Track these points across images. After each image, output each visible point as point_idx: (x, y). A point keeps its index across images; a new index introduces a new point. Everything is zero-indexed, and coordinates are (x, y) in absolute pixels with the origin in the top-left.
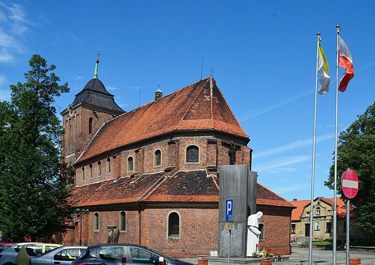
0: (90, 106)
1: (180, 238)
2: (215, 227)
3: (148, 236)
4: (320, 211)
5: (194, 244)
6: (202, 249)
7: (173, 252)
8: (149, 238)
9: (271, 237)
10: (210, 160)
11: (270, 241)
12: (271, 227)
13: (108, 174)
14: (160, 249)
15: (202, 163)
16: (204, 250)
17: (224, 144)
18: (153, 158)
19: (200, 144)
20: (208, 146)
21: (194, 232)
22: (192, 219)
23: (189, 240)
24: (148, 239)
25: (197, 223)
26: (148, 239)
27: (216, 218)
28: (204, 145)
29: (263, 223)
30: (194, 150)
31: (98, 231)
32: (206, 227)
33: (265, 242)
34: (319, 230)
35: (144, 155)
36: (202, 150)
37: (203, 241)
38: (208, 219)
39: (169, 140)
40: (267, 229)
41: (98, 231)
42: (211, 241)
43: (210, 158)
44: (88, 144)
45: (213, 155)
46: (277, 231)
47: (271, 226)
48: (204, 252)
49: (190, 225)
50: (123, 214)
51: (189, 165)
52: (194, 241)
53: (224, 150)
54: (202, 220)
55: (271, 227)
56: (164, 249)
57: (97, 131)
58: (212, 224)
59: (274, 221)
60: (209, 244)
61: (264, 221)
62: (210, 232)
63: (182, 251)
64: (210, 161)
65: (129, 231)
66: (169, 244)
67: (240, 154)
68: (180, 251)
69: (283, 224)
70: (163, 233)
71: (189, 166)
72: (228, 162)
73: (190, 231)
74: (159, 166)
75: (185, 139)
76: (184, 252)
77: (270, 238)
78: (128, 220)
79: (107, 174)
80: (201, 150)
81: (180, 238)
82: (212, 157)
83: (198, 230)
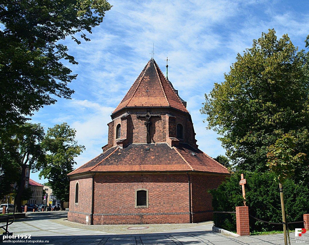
9: (158, 203)
17: (139, 118)
29: (145, 190)
33: (149, 208)
46: (168, 197)
53: (140, 123)
77: (158, 204)
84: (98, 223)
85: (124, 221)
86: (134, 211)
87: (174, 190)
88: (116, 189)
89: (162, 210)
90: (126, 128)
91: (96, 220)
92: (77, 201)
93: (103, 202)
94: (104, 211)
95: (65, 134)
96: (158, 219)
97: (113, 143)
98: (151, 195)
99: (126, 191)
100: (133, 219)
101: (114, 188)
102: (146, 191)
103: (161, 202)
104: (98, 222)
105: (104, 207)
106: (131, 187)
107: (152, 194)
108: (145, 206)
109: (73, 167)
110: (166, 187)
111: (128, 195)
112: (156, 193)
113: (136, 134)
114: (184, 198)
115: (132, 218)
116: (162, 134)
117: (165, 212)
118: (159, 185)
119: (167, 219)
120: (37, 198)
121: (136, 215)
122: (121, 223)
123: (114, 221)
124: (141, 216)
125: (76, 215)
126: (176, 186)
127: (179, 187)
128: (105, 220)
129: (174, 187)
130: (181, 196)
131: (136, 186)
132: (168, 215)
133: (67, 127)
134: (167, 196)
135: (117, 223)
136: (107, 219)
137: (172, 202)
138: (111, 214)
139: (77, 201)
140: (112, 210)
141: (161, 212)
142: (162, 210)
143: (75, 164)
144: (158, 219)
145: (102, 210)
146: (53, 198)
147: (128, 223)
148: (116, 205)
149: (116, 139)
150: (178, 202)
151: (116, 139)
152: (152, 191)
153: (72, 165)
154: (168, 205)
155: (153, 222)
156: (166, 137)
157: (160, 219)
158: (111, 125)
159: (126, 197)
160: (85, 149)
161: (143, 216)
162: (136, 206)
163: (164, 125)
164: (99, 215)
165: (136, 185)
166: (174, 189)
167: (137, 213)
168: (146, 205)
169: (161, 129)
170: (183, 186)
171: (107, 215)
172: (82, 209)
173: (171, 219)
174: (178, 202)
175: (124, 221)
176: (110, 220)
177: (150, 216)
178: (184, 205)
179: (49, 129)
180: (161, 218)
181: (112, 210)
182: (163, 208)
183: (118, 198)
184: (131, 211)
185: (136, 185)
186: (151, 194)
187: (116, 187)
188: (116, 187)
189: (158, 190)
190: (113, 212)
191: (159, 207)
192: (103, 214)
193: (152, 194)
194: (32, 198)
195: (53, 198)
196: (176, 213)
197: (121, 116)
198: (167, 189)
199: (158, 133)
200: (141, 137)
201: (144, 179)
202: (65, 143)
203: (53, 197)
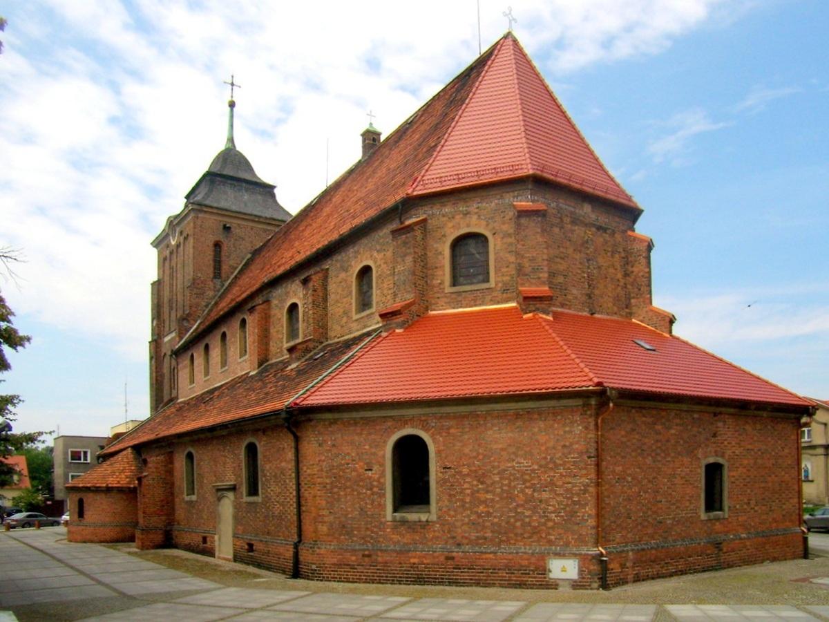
0: (215, 211)
1: (434, 517)
2: (562, 475)
3: (325, 512)
4: (809, 431)
5: (487, 535)
6: (517, 553)
7: (412, 561)
8: (326, 519)
9: (745, 503)
10: (528, 270)
11: (745, 518)
12: (745, 470)
13: (242, 359)
14: (367, 553)
15: (500, 285)
16: (525, 556)
18: (351, 293)
19: (491, 227)
20: (518, 226)
21: (483, 496)
22: (475, 454)
23: (468, 524)
24: (325, 522)
25: (493, 467)
26: (325, 522)
27: (564, 446)
28: (505, 227)
29: (721, 460)
30: (472, 247)
31: (194, 498)
32: (527, 477)
34: (812, 481)
35: (326, 289)
36: (499, 242)
37: (518, 524)
38: (535, 451)
39: (395, 225)
40: (733, 479)
41: (194, 498)
42: (550, 524)
43: (527, 265)
44: (210, 303)
45: (534, 255)
46: (763, 485)
47: (745, 467)
48: (526, 563)
49: (468, 475)
50: (252, 450)
51: (459, 293)
52: (484, 527)
53: (568, 243)
54: (513, 457)
55: (745, 470)
56: (379, 553)
57: (232, 273)
58: (552, 469)
59: (752, 453)
60: (544, 535)
61: (724, 453)
62: (545, 496)
63: (442, 559)
64: (526, 275)
65: (267, 499)
66: (396, 537)
67: (617, 256)
68: (437, 557)
69: (780, 461)
70: (373, 502)
71: (460, 299)
72: (583, 280)
73: (468, 491)
74: (368, 312)
75: (444, 216)
76: (450, 562)
78: (266, 467)
79: (240, 360)
80: (495, 245)
81: (434, 517)
82: (533, 260)
83: (498, 490)
88: (659, 458)
89: (752, 524)
101: (653, 454)
105: (629, 521)
110: (759, 453)
122: (676, 572)
128: (637, 567)
131: (703, 449)
147: (690, 570)
148: (660, 511)
162: (703, 516)
176: (650, 565)
181: (650, 531)
200: (575, 291)
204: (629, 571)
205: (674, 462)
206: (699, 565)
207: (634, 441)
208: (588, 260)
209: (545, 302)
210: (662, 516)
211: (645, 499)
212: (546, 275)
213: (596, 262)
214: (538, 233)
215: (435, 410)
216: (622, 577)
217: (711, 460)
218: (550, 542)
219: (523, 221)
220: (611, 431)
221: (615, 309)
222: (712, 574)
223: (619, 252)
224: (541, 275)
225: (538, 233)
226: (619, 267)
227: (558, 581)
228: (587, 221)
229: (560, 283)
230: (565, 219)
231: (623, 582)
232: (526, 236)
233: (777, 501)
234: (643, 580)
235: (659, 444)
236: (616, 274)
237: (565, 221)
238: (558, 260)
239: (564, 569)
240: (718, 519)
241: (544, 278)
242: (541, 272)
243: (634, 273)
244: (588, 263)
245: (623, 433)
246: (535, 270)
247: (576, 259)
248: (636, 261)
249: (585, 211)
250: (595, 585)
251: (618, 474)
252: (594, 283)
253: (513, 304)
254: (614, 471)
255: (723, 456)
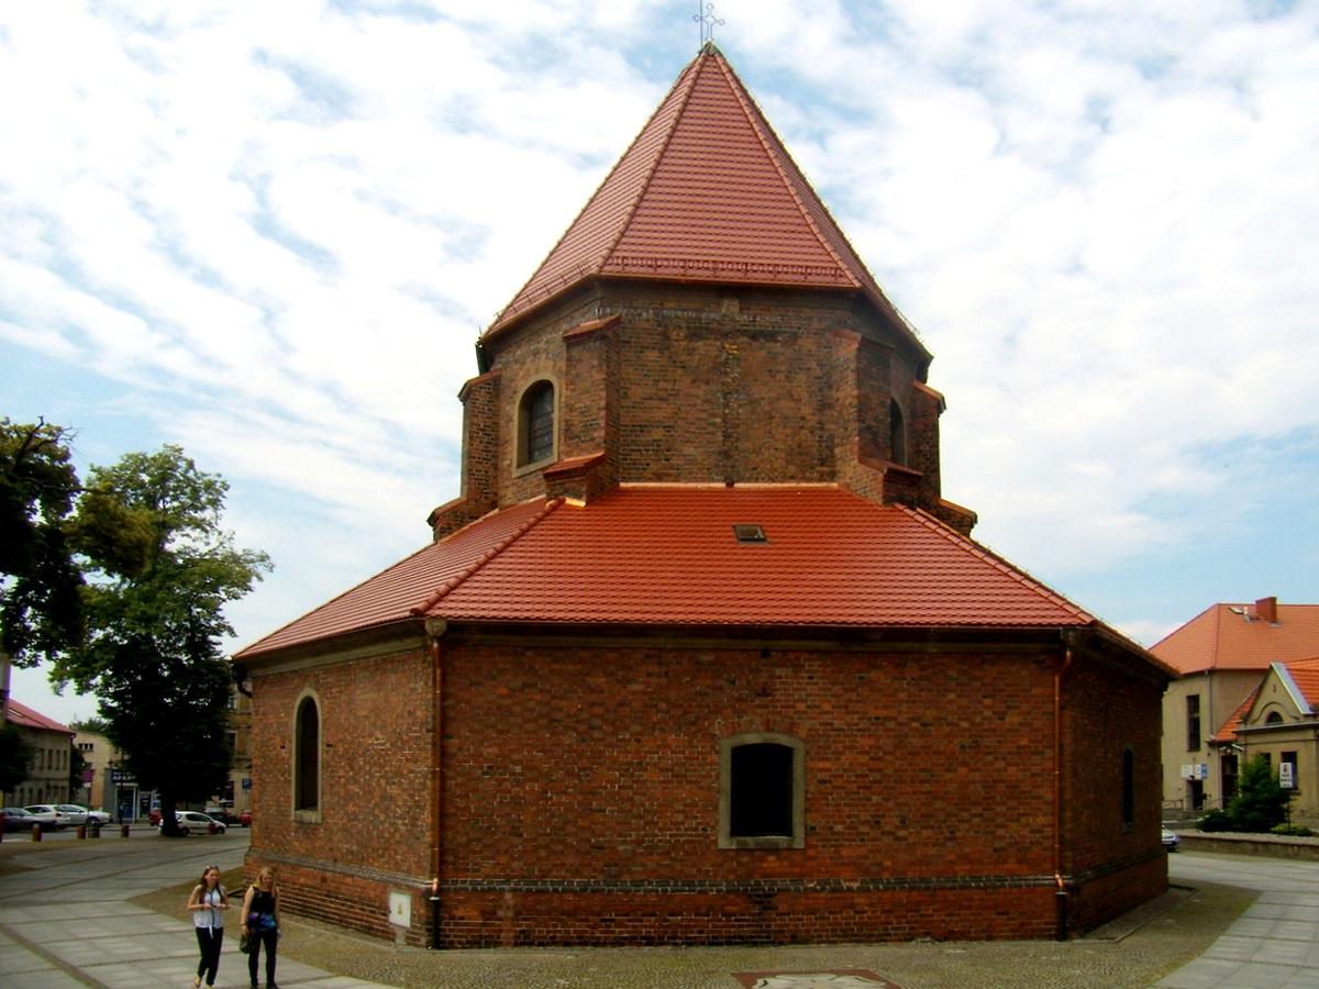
29: (783, 740)
33: (811, 852)
46: (927, 787)
53: (680, 371)
59: (891, 725)
77: (864, 829)
84: (481, 936)
85: (654, 926)
86: (713, 866)
87: (963, 747)
88: (597, 735)
90: (603, 394)
91: (463, 918)
92: (307, 799)
93: (508, 810)
94: (515, 865)
95: (175, 498)
96: (864, 912)
97: (496, 494)
98: (820, 776)
99: (659, 746)
100: (707, 915)
101: (582, 728)
102: (787, 753)
103: (883, 816)
104: (479, 931)
105: (516, 840)
106: (694, 724)
107: (828, 765)
108: (781, 840)
109: (218, 648)
110: (914, 724)
111: (672, 770)
112: (851, 765)
113: (658, 434)
114: (1024, 792)
115: (703, 910)
116: (810, 437)
117: (910, 873)
118: (872, 713)
119: (922, 916)
120: (48, 779)
121: (728, 892)
123: (581, 926)
124: (760, 896)
125: (307, 876)
126: (980, 724)
127: (994, 730)
129: (965, 725)
130: (1003, 781)
131: (725, 718)
132: (927, 889)
133: (183, 464)
134: (921, 782)
135: (606, 938)
136: (539, 912)
137: (949, 815)
138: (561, 883)
139: (307, 799)
140: (570, 860)
141: (886, 876)
142: (888, 863)
143: (225, 634)
144: (864, 912)
145: (503, 860)
146: (122, 781)
147: (675, 938)
149: (519, 467)
150: (987, 814)
151: (519, 467)
152: (829, 747)
153: (212, 638)
154: (925, 833)
155: (832, 930)
156: (834, 457)
157: (876, 917)
158: (482, 398)
159: (662, 782)
160: (271, 568)
161: (773, 900)
162: (724, 842)
163: (826, 391)
164: (482, 890)
165: (728, 712)
166: (967, 742)
167: (731, 877)
168: (787, 830)
169: (806, 411)
170: (1020, 724)
171: (538, 891)
172: (355, 848)
173: (950, 915)
174: (987, 814)
175: (648, 926)
176: (561, 921)
177: (816, 895)
178: (1026, 832)
179: (93, 470)
180: (883, 911)
181: (570, 860)
182: (897, 850)
183: (605, 787)
184: (694, 865)
185: (726, 712)
186: (821, 765)
187: (596, 722)
188: (596, 722)
189: (865, 742)
190: (577, 873)
191: (870, 845)
192: (508, 882)
193: (828, 765)
194: (27, 778)
195: (122, 781)
196: (977, 879)
197: (566, 327)
198: (923, 736)
199: (789, 431)
200: (690, 450)
201: (780, 677)
202: (177, 542)
203: (122, 775)
204: (506, 925)
205: (638, 741)
206: (701, 932)
207: (532, 704)
208: (725, 395)
209: (577, 479)
210: (603, 836)
211: (559, 804)
212: (602, 433)
213: (748, 394)
214: (593, 367)
215: (329, 658)
216: (484, 933)
217: (752, 739)
218: (397, 867)
219: (575, 352)
220: (473, 688)
221: (792, 469)
222: (587, 953)
223: (808, 369)
224: (596, 435)
225: (593, 367)
226: (805, 397)
227: (396, 929)
228: (727, 329)
229: (654, 441)
230: (674, 335)
231: (486, 942)
232: (577, 375)
233: (976, 820)
234: (540, 944)
235: (598, 710)
236: (800, 409)
237: (673, 337)
238: (654, 403)
239: (401, 909)
240: (774, 850)
241: (600, 437)
242: (595, 430)
243: (840, 401)
244: (725, 398)
245: (504, 691)
246: (588, 427)
247: (697, 397)
248: (842, 380)
249: (724, 311)
250: (423, 940)
251: (486, 760)
252: (740, 430)
253: (622, 485)
254: (477, 756)
255: (790, 730)
